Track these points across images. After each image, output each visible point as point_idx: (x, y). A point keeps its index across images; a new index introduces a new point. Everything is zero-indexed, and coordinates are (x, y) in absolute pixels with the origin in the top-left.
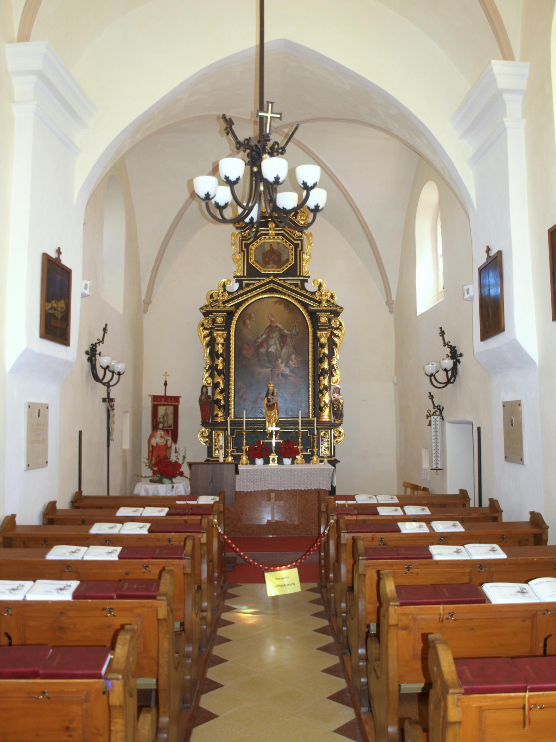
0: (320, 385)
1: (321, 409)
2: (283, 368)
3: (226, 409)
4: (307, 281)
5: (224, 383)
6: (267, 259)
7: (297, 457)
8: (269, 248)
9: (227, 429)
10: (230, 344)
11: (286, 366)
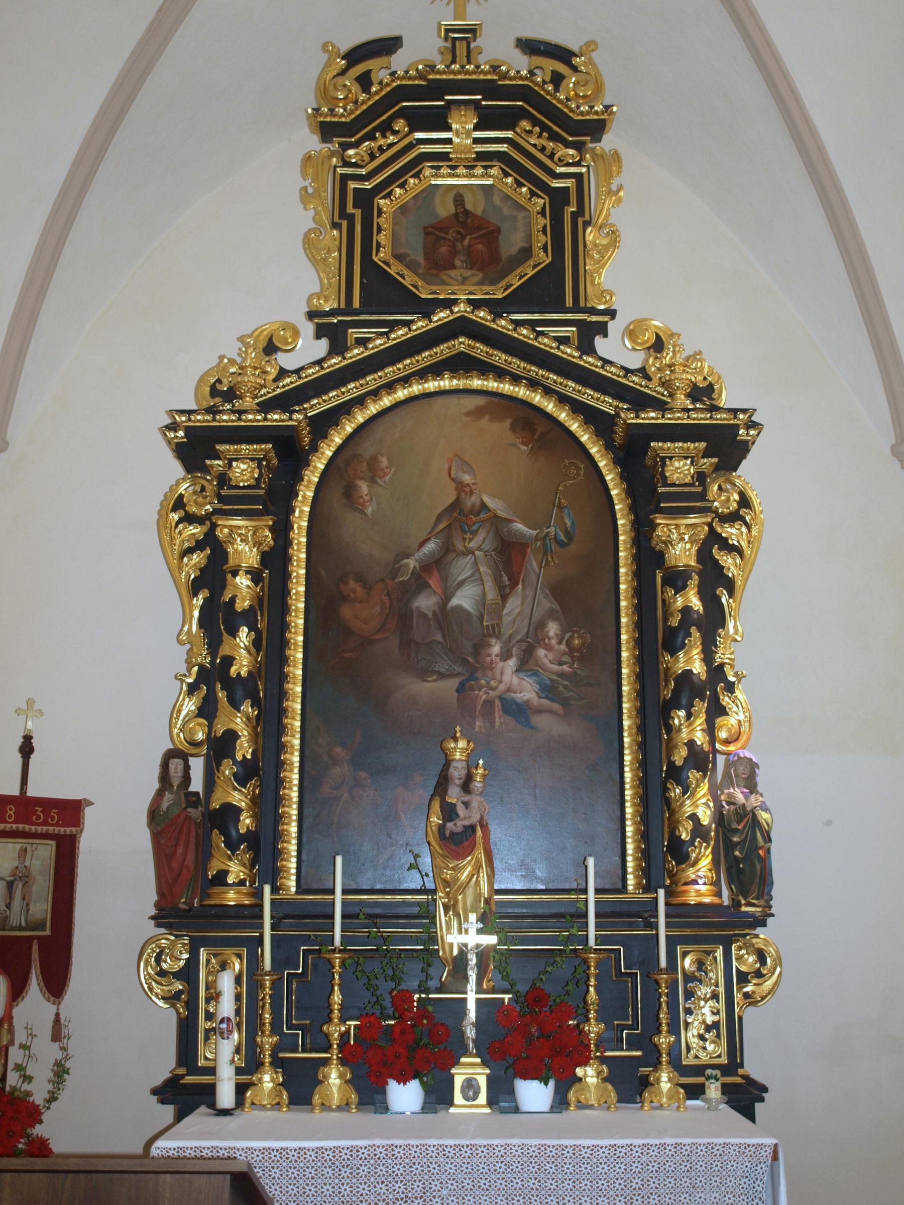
0: (671, 747)
1: (679, 852)
2: (509, 678)
3: (263, 849)
4: (602, 330)
5: (254, 737)
6: (444, 250)
7: (579, 1071)
8: (452, 210)
9: (260, 941)
10: (285, 576)
11: (520, 669)
